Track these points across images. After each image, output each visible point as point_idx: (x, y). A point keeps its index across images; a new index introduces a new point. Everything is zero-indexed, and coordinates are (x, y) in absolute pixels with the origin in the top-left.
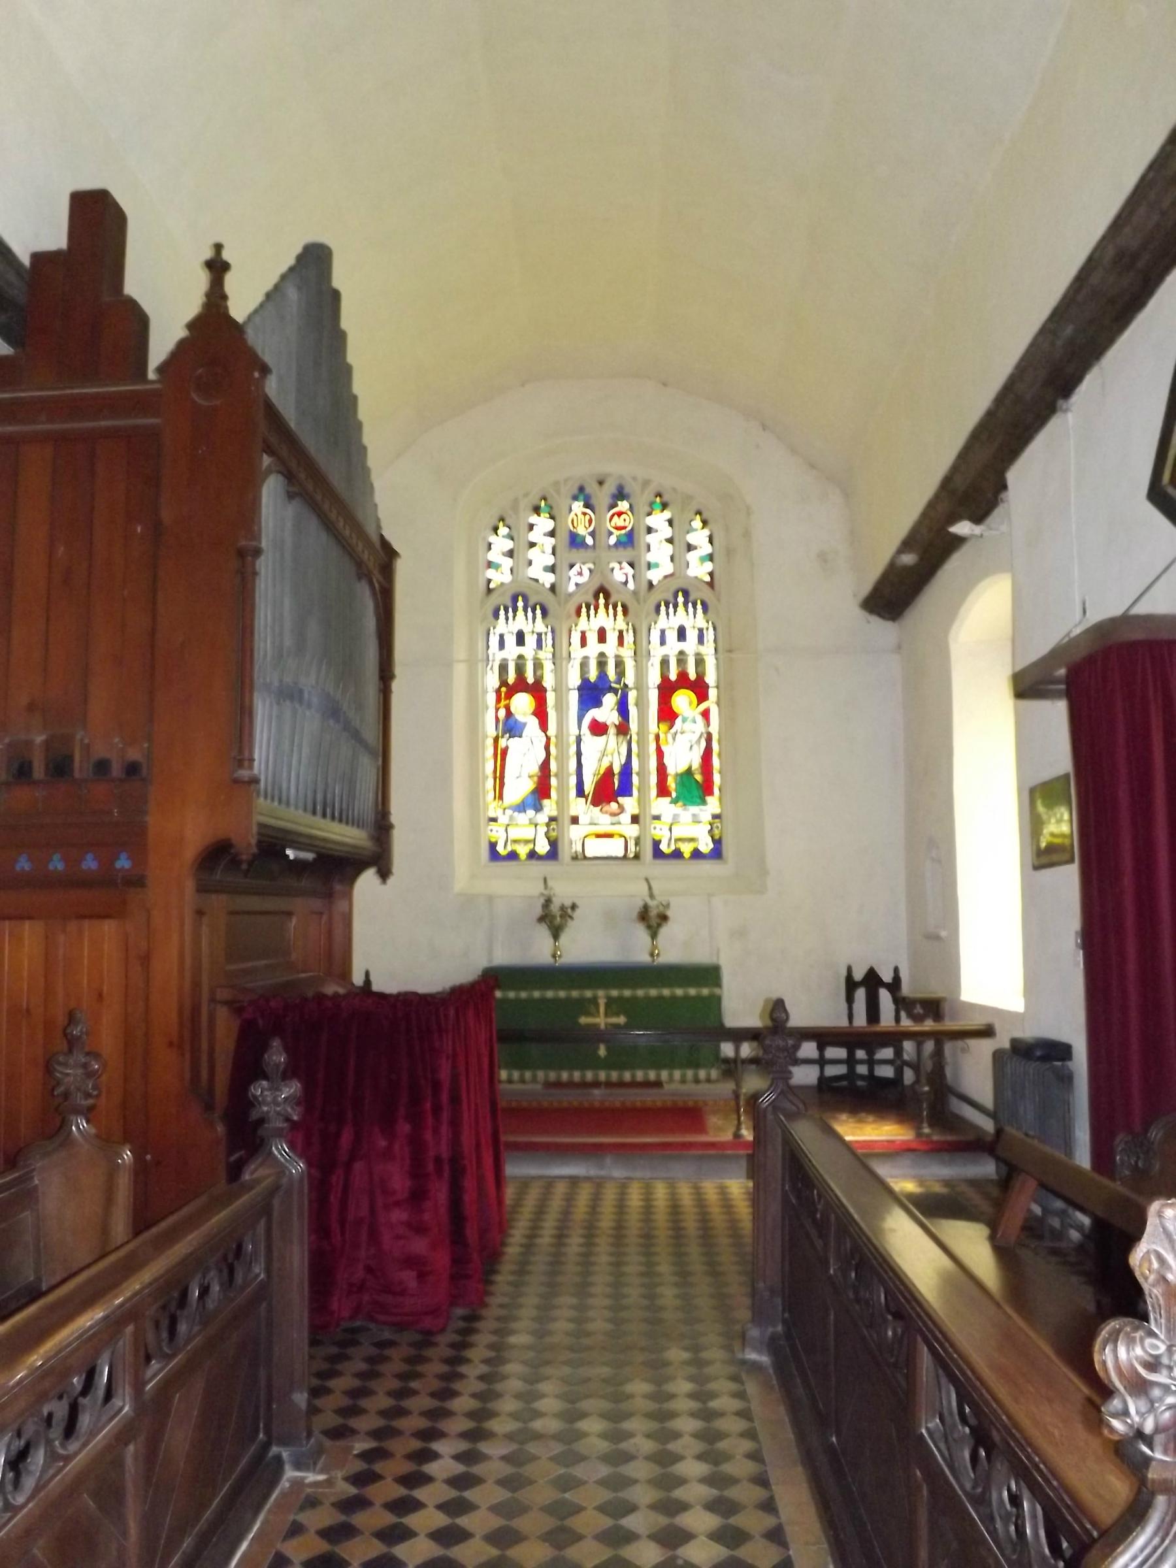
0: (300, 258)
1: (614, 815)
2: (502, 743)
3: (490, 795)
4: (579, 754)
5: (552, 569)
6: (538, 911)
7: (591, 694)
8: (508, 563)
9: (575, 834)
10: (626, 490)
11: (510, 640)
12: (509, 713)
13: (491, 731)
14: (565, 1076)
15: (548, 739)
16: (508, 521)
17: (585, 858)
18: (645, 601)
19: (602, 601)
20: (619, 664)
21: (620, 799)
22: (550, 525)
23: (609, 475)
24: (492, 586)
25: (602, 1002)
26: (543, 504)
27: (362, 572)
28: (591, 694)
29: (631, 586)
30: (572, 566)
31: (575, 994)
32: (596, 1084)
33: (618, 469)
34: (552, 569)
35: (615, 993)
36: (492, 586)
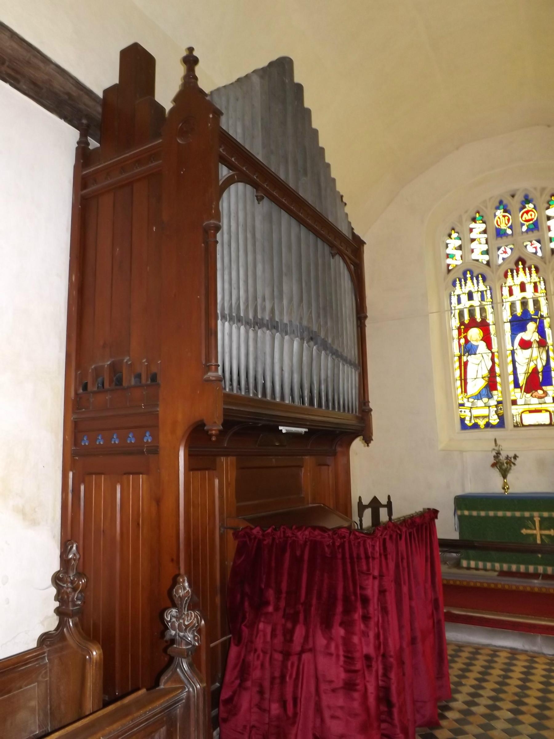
0: (271, 64)
1: (540, 398)
2: (464, 359)
3: (459, 390)
4: (514, 362)
5: (487, 252)
6: (492, 461)
7: (518, 324)
8: (459, 253)
9: (515, 410)
10: (530, 197)
11: (464, 298)
12: (467, 341)
13: (457, 352)
14: (514, 568)
15: (493, 354)
16: (456, 230)
17: (524, 426)
18: (549, 262)
19: (521, 266)
20: (536, 302)
21: (544, 388)
22: (483, 226)
23: (518, 190)
24: (450, 268)
25: (537, 520)
26: (477, 215)
27: (335, 251)
28: (518, 324)
29: (540, 254)
30: (499, 249)
31: (518, 514)
32: (536, 575)
33: (523, 185)
34: (487, 252)
35: (546, 514)
36: (450, 268)
